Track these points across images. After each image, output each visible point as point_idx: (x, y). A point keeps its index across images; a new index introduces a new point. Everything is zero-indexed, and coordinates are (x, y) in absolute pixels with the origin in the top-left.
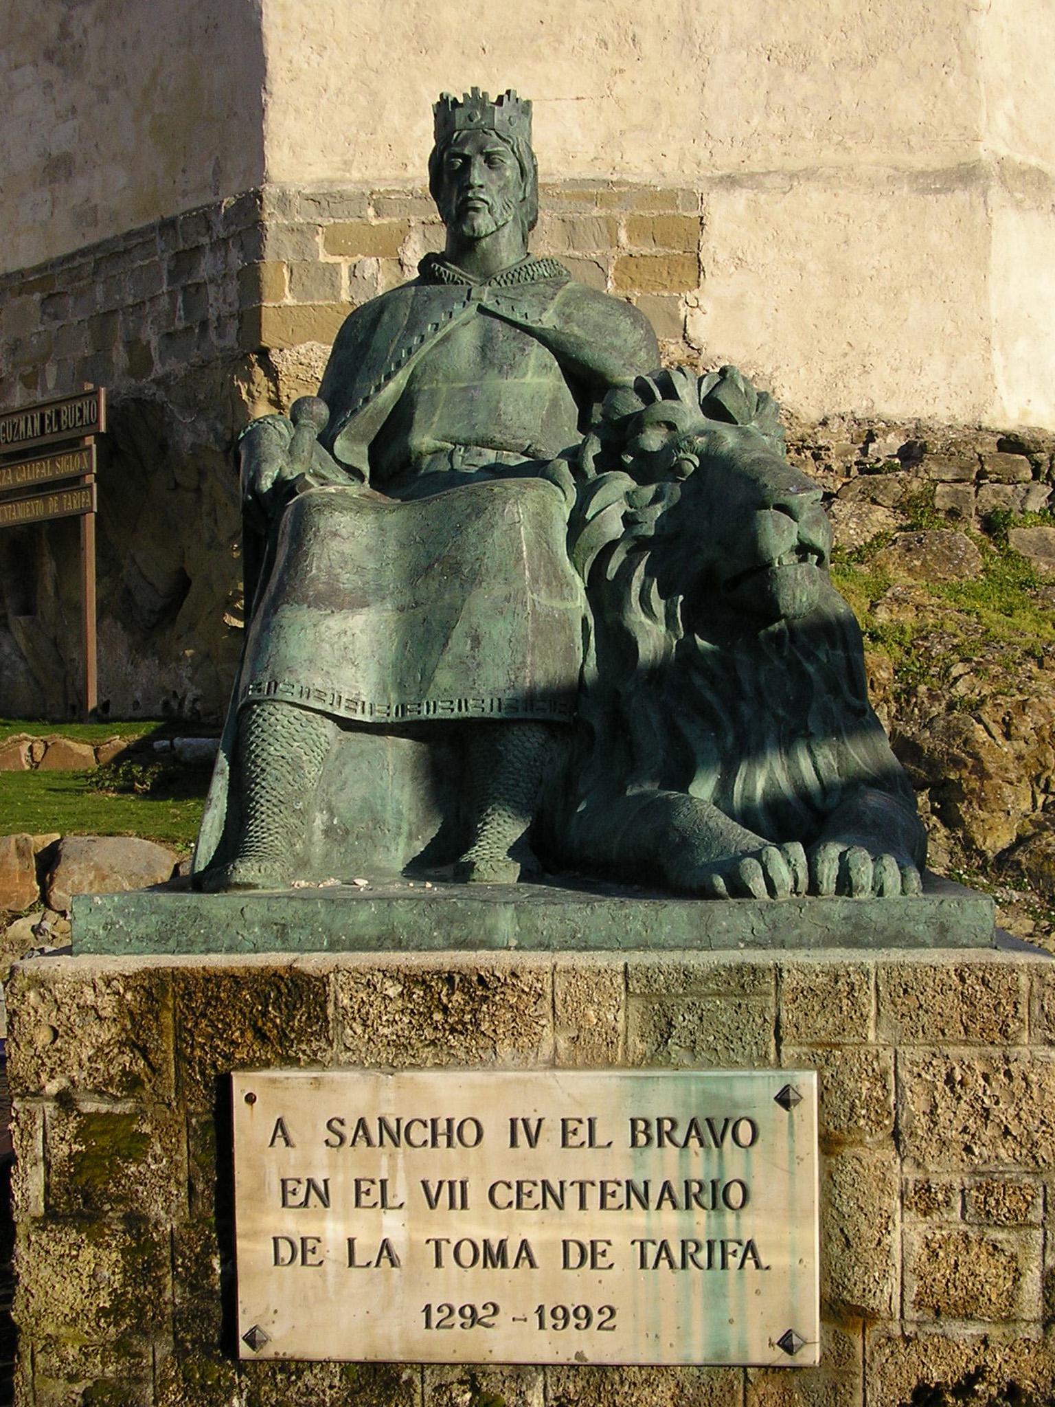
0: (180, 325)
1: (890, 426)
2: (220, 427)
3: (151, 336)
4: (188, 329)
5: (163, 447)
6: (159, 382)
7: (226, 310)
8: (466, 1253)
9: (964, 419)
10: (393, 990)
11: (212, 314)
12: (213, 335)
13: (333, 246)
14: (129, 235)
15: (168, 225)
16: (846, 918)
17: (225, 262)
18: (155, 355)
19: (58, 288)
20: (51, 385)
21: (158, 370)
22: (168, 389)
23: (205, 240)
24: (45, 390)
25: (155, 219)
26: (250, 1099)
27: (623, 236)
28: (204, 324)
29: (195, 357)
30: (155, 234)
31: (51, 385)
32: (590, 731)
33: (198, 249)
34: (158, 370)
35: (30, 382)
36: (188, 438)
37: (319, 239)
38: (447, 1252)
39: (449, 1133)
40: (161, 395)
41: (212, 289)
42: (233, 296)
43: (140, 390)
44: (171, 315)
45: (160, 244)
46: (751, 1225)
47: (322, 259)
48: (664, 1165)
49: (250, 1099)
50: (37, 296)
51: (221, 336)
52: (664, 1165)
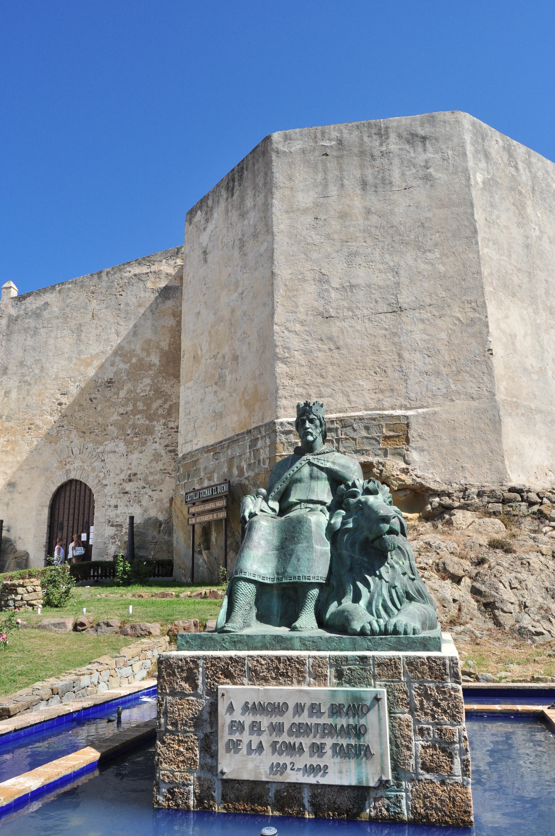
3: (244, 465)
6: (246, 479)
11: (261, 458)
12: (262, 464)
14: (238, 435)
15: (249, 432)
18: (245, 470)
19: (218, 451)
21: (246, 475)
23: (259, 436)
24: (214, 481)
25: (245, 430)
28: (259, 461)
33: (258, 439)
35: (209, 479)
40: (247, 482)
42: (267, 453)
44: (249, 458)
48: (342, 721)
49: (223, 695)
50: (212, 453)
52: (342, 721)
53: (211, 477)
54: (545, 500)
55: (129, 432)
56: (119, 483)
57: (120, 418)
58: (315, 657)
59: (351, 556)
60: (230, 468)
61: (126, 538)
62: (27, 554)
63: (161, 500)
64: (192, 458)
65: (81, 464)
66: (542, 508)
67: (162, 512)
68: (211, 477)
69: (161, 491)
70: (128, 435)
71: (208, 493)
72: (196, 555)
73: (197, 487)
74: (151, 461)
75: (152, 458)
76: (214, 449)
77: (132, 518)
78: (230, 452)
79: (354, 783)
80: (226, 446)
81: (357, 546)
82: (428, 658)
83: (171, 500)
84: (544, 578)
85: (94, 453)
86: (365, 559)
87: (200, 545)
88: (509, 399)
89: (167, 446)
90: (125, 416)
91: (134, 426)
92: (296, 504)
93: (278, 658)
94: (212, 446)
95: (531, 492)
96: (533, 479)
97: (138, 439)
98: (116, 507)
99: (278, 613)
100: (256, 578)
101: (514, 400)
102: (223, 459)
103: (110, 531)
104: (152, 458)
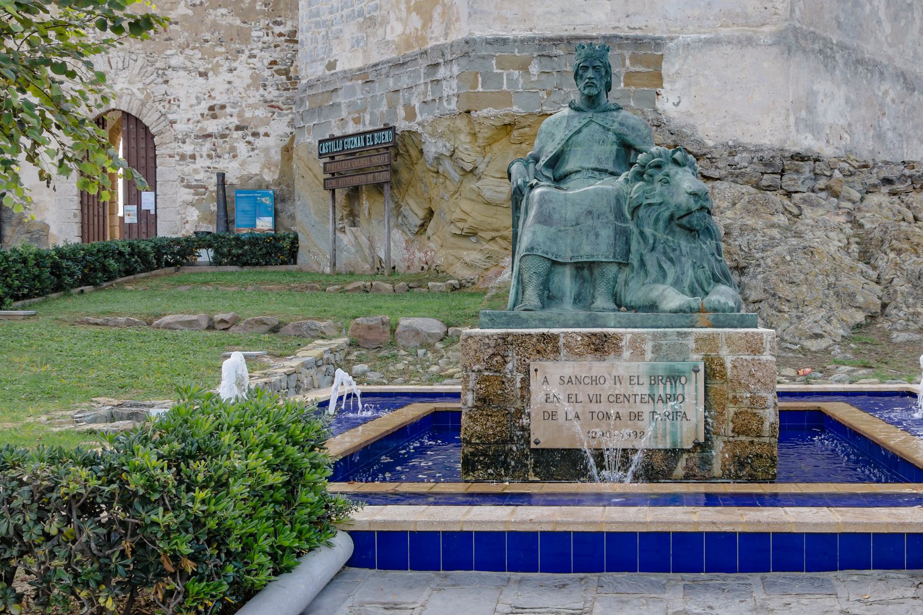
0: (429, 98)
1: (745, 149)
2: (448, 145)
3: (416, 103)
4: (434, 100)
5: (421, 151)
7: (451, 93)
8: (601, 416)
9: (777, 145)
10: (579, 338)
11: (445, 94)
12: (445, 104)
13: (500, 65)
16: (694, 194)
17: (451, 71)
18: (417, 111)
19: (370, 78)
20: (367, 123)
22: (424, 127)
23: (441, 61)
24: (364, 125)
26: (536, 370)
27: (628, 62)
29: (437, 112)
30: (418, 57)
31: (367, 123)
32: (633, 267)
34: (419, 118)
35: (357, 121)
36: (433, 150)
37: (494, 62)
38: (595, 415)
39: (595, 381)
40: (420, 130)
41: (444, 83)
42: (454, 86)
43: (411, 127)
44: (425, 93)
45: (420, 61)
46: (683, 408)
47: (495, 71)
49: (536, 370)
50: (360, 82)
51: (449, 104)
53: (359, 118)
54: (837, 173)
55: (208, 36)
56: (196, 119)
57: (190, 12)
58: (633, 333)
59: (653, 235)
60: (392, 107)
61: (214, 207)
62: (47, 227)
63: (267, 150)
64: (328, 88)
65: (126, 85)
66: (832, 183)
67: (269, 169)
68: (359, 118)
69: (266, 135)
70: (207, 41)
71: (358, 143)
72: (338, 233)
73: (337, 133)
74: (248, 86)
75: (250, 81)
76: (366, 76)
77: (222, 176)
78: (391, 81)
79: (668, 447)
80: (384, 71)
81: (661, 223)
82: (746, 334)
83: (287, 150)
84: (519, 401)
85: (149, 69)
86: (670, 238)
87: (342, 219)
88: (805, 27)
89: (274, 63)
90: (199, 8)
91: (215, 27)
92: (577, 172)
93: (594, 335)
94: (360, 70)
95: (819, 161)
96: (822, 144)
97: (223, 50)
98: (193, 157)
99: (571, 292)
100: (549, 256)
101: (812, 29)
102: (378, 90)
103: (186, 195)
104: (250, 81)
